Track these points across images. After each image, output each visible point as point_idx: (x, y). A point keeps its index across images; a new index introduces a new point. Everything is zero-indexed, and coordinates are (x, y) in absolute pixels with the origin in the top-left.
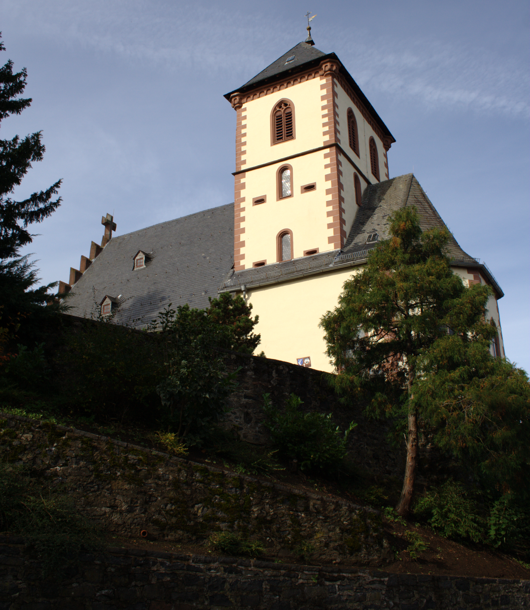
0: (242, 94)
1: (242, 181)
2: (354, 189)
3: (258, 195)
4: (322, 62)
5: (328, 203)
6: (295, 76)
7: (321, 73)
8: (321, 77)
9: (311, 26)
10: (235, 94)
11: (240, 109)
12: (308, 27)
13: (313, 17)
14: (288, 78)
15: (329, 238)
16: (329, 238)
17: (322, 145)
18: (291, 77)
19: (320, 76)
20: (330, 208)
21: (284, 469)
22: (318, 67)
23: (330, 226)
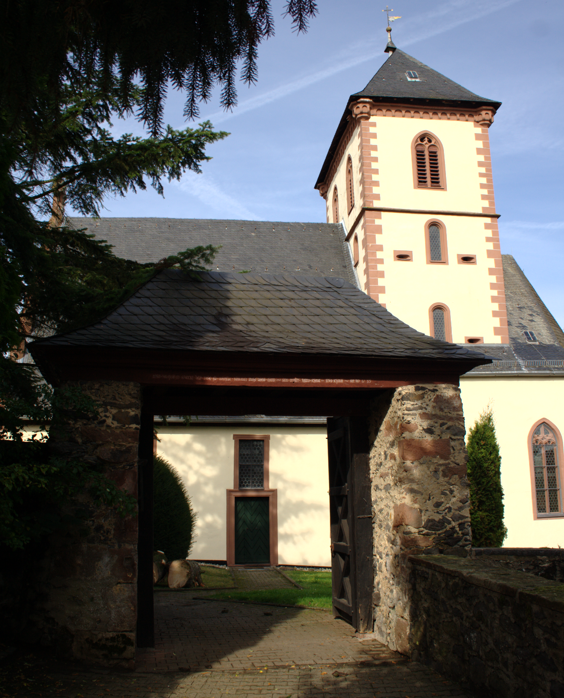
0: (374, 103)
1: (377, 222)
2: (373, 212)
3: (403, 248)
4: (484, 107)
5: (493, 286)
6: (445, 108)
7: (477, 118)
8: (476, 123)
9: (391, 27)
10: (368, 100)
11: (366, 121)
12: (387, 27)
13: (396, 18)
14: (436, 108)
15: (495, 328)
16: (495, 328)
17: (480, 211)
18: (439, 108)
19: (475, 121)
20: (495, 293)
21: (26, 285)
22: (475, 110)
23: (495, 314)
